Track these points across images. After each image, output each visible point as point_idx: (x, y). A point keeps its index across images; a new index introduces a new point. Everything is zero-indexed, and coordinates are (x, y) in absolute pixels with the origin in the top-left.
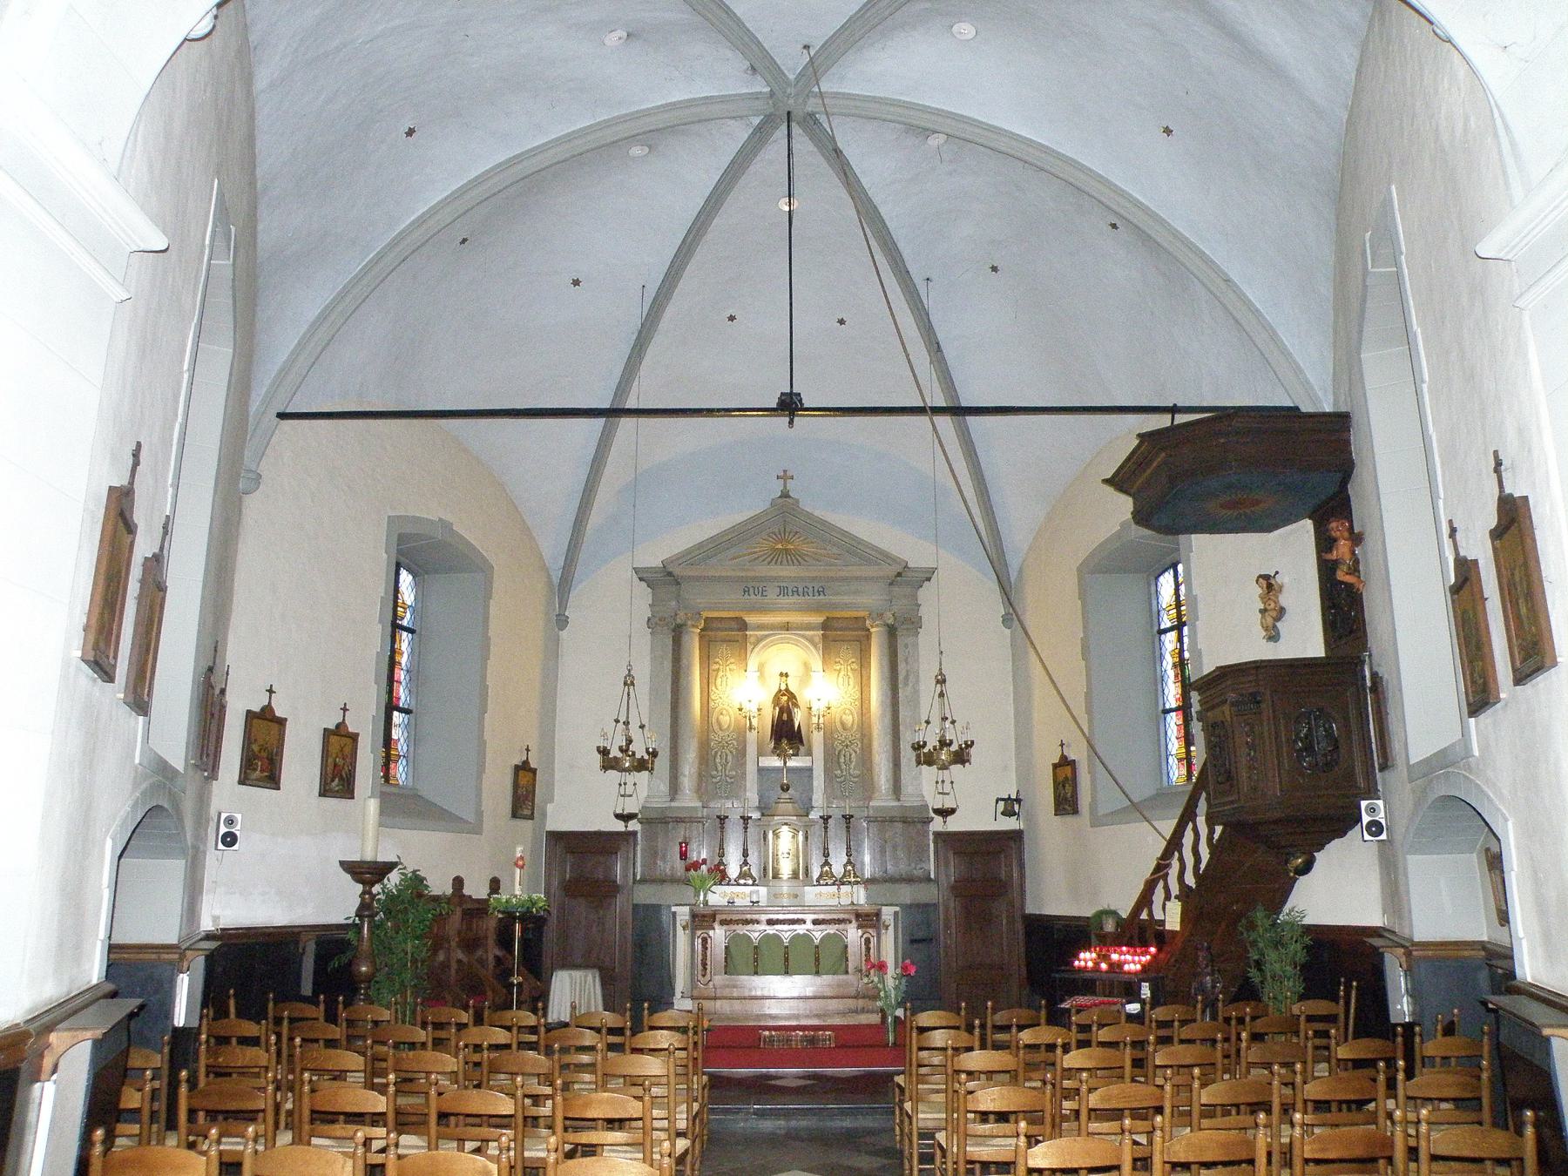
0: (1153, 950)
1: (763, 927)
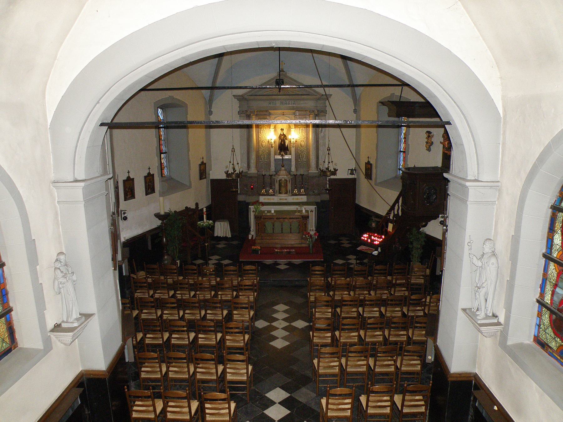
0: (383, 237)
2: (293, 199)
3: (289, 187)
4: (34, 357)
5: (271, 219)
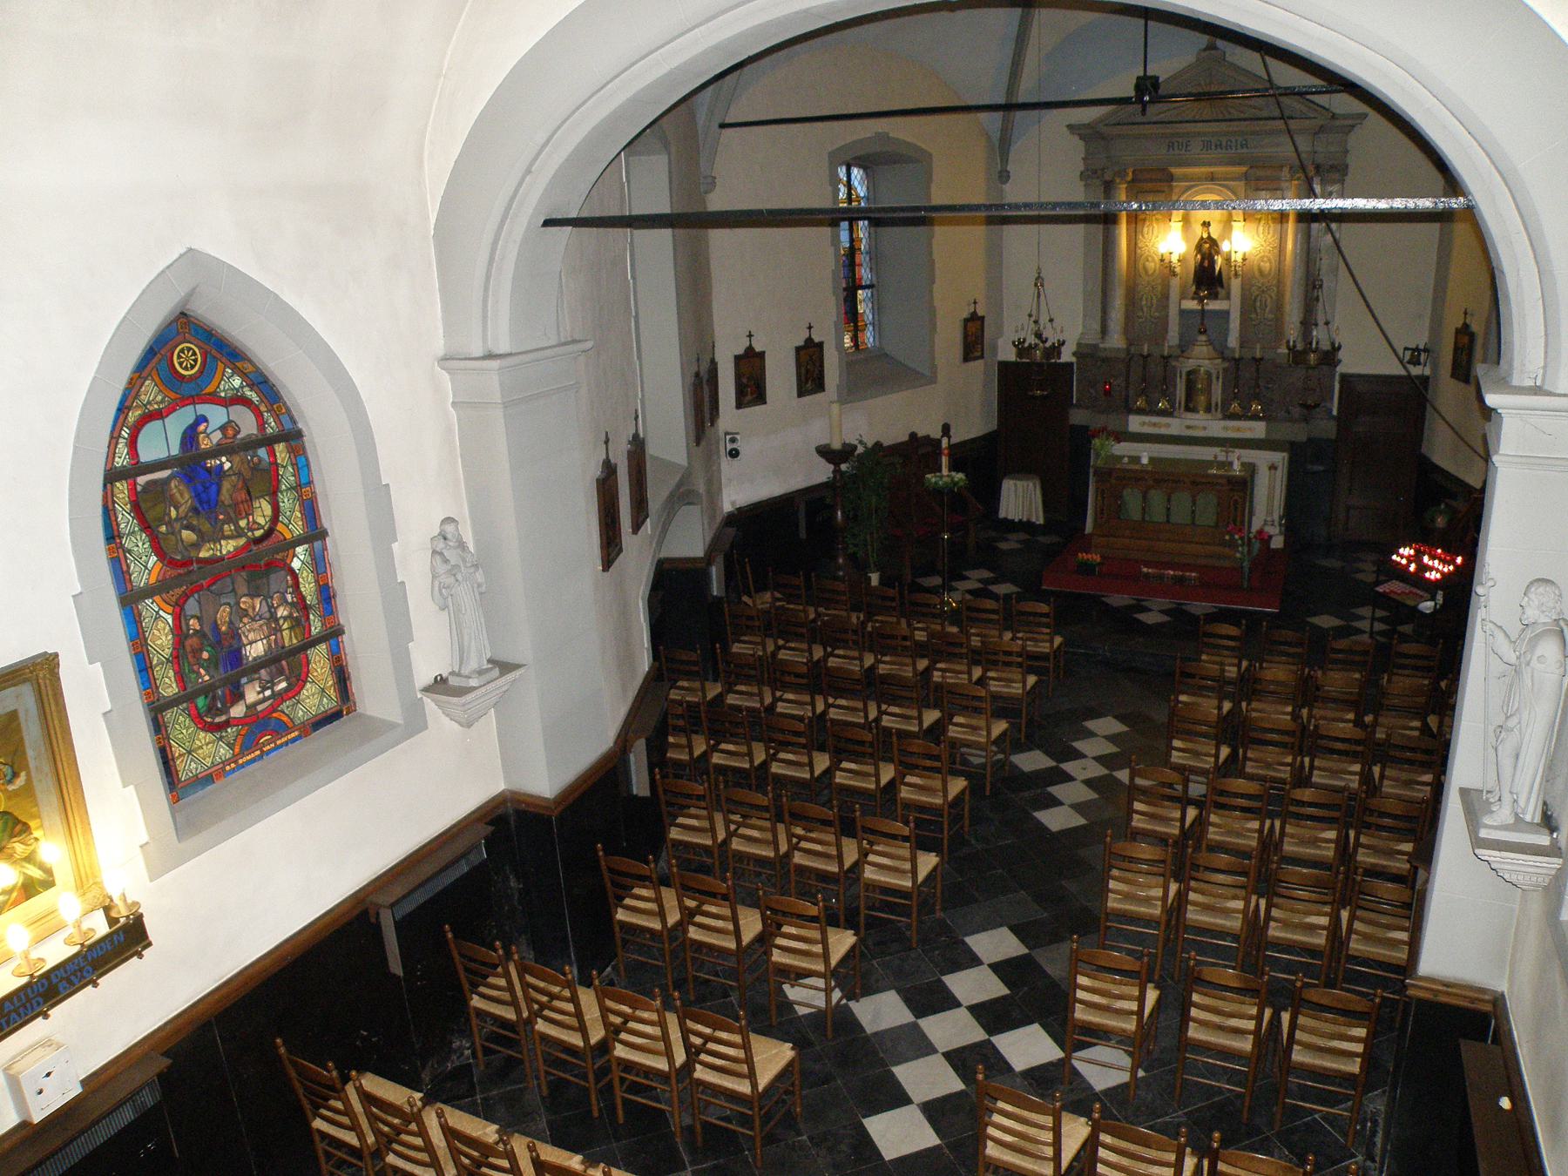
2: (1226, 428)
3: (1217, 393)
4: (378, 735)
5: (1137, 480)
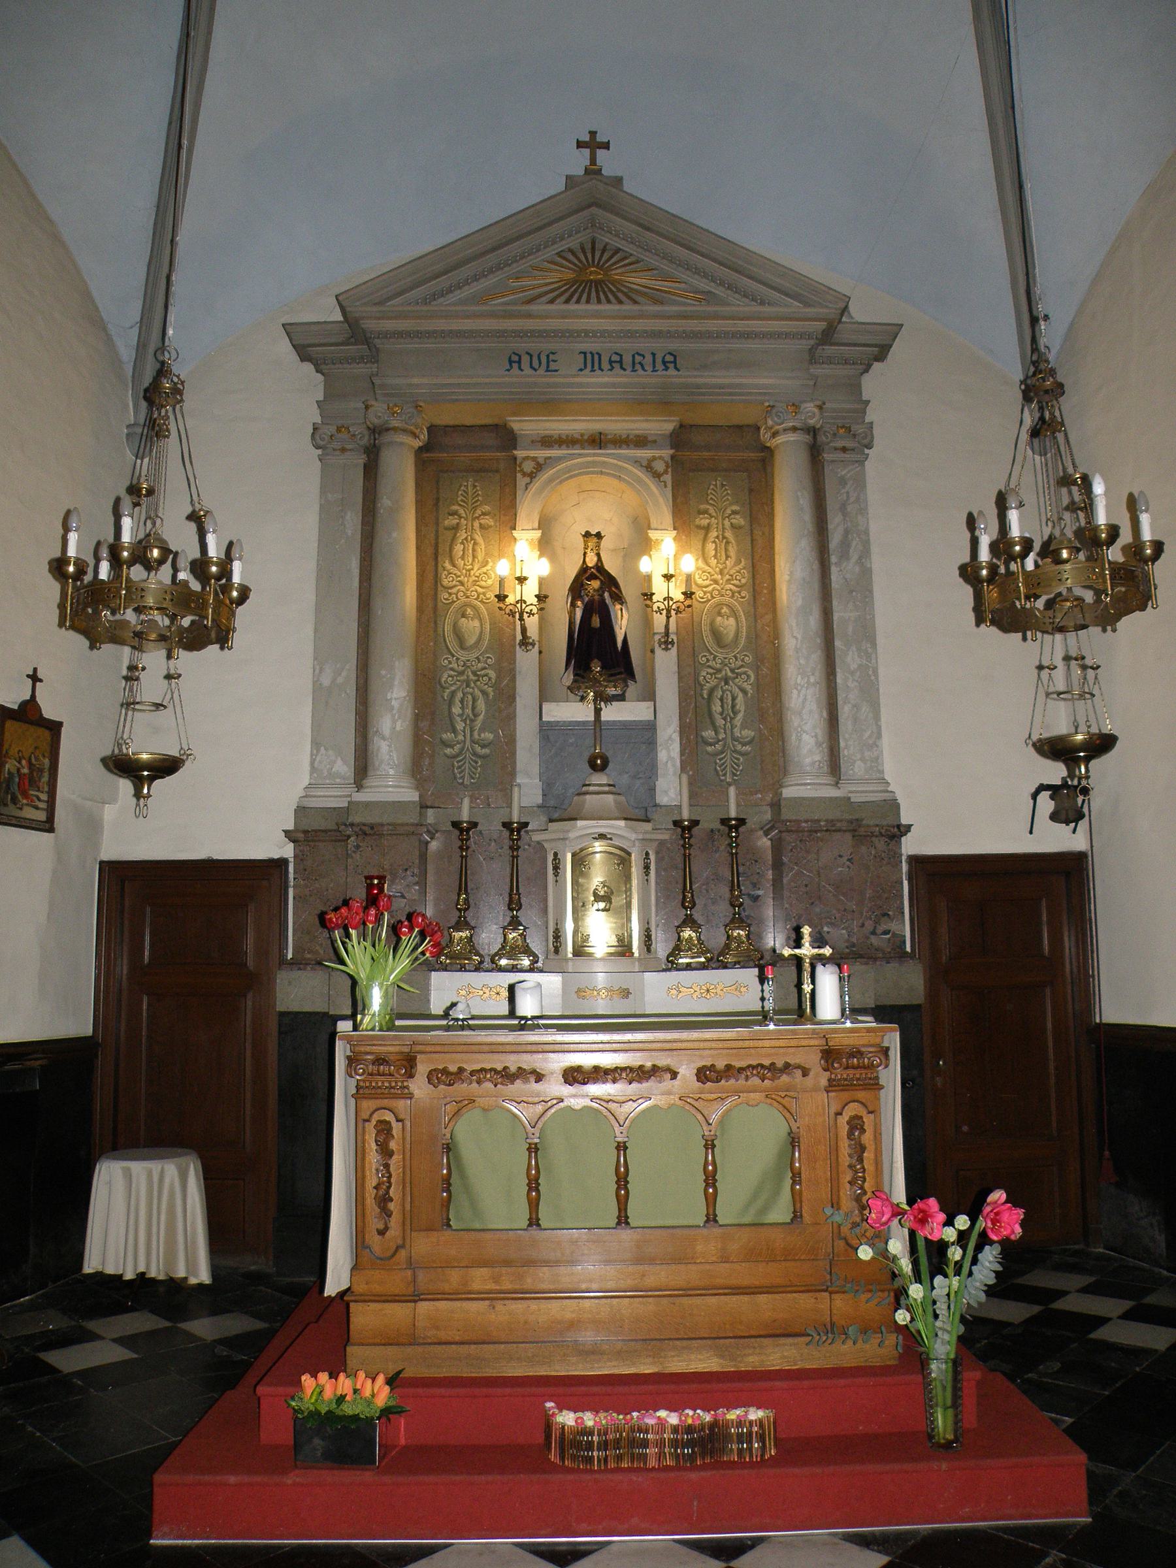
1: (555, 1087)
